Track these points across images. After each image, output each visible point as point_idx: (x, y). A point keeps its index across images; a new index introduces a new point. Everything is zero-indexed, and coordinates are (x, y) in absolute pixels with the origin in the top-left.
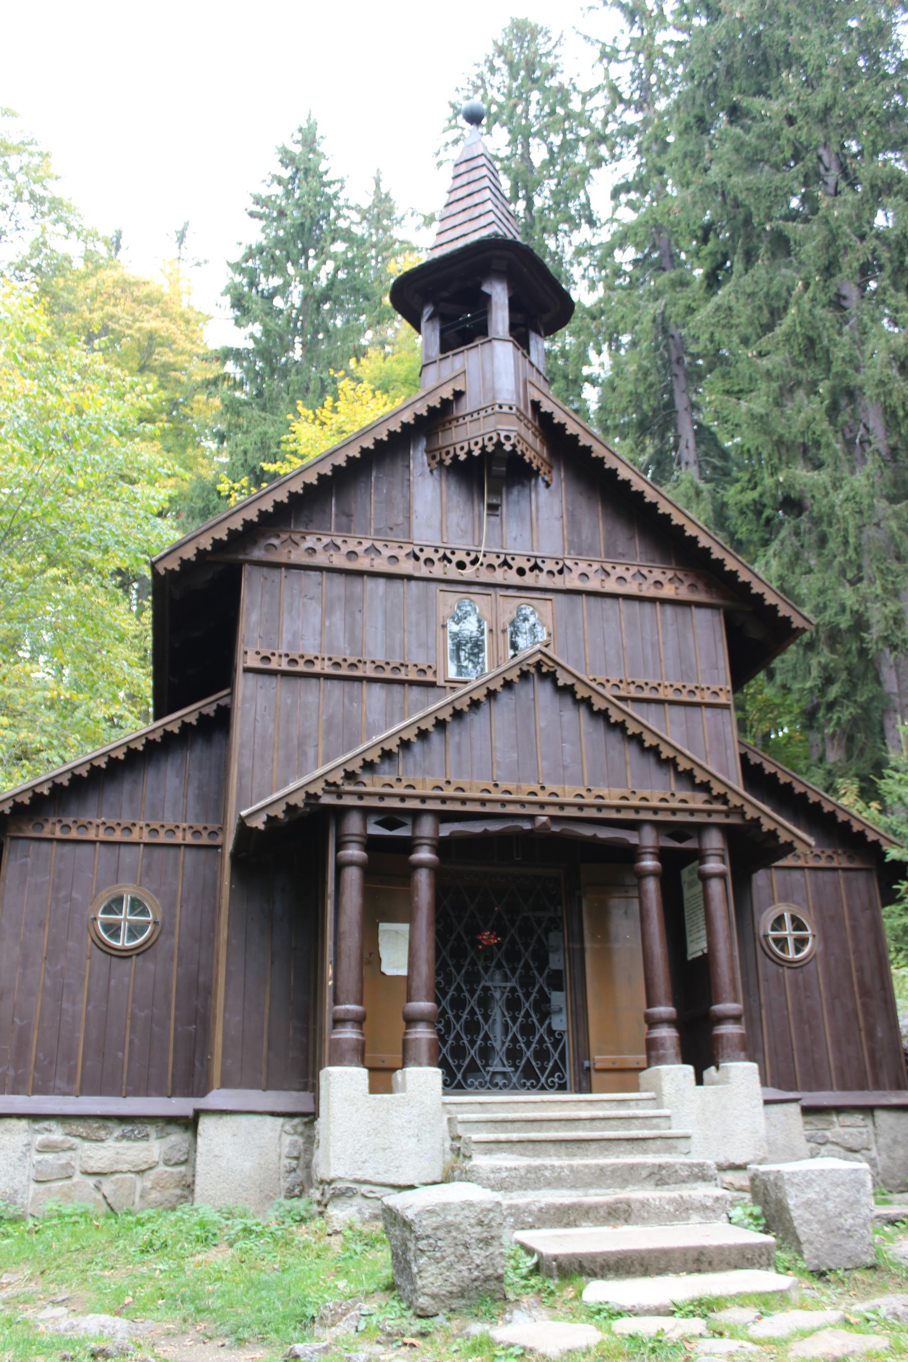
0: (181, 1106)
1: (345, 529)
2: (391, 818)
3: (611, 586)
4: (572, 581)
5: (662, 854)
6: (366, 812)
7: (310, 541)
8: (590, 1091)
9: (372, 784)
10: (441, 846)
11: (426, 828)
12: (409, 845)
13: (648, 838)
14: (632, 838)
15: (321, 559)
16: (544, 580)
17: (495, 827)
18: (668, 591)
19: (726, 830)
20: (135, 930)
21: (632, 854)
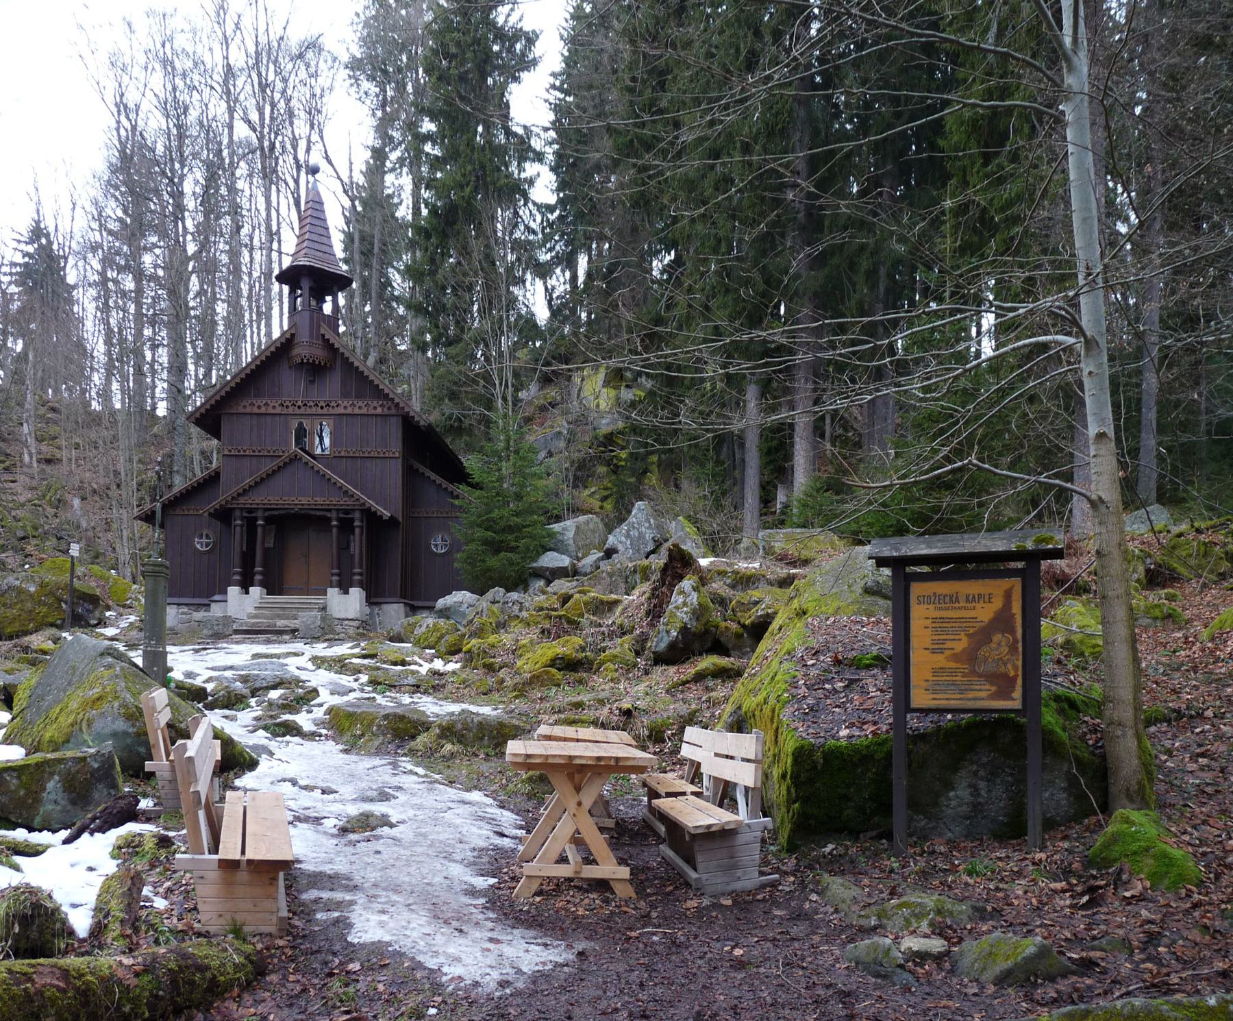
0: (206, 601)
1: (257, 396)
2: (250, 511)
3: (357, 411)
4: (341, 410)
5: (339, 519)
6: (242, 509)
7: (244, 403)
8: (281, 593)
9: (242, 500)
10: (266, 519)
11: (260, 514)
12: (330, 519)
13: (334, 515)
14: (329, 515)
15: (248, 410)
16: (332, 411)
17: (282, 512)
18: (379, 410)
19: (362, 511)
20: (207, 545)
21: (330, 519)
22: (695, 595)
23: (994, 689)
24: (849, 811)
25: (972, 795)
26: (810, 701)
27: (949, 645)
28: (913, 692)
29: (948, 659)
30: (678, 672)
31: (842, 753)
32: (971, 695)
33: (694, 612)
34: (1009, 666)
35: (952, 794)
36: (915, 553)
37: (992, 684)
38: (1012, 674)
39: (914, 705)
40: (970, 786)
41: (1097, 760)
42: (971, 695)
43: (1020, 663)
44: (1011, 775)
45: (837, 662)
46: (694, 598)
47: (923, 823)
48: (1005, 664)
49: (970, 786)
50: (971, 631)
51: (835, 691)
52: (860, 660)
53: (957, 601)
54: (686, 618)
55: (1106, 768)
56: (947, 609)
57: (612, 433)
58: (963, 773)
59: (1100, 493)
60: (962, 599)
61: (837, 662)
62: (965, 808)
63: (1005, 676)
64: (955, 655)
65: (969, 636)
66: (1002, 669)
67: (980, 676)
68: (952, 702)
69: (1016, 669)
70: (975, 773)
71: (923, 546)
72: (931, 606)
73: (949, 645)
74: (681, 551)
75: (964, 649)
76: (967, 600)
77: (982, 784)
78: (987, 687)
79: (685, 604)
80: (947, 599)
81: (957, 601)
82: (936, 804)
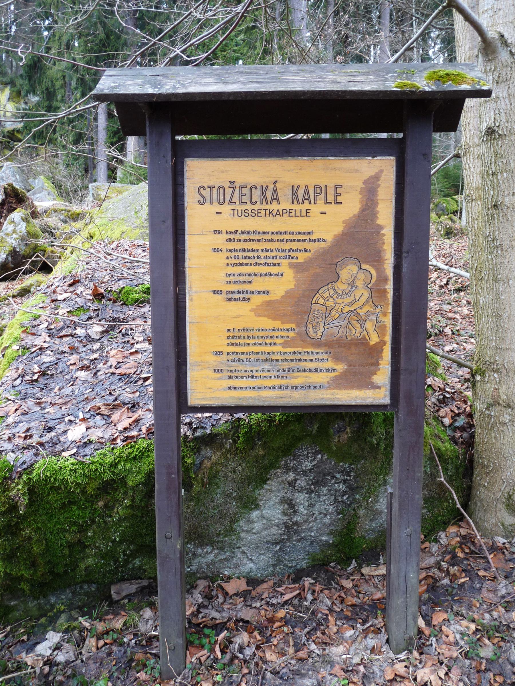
22: (24, 225)
23: (341, 367)
24: (91, 561)
25: (284, 514)
26: (48, 358)
27: (259, 284)
28: (192, 375)
29: (258, 312)
30: (7, 287)
31: (64, 482)
32: (300, 379)
33: (22, 239)
34: (369, 326)
35: (255, 514)
36: (191, 89)
37: (337, 359)
38: (374, 339)
39: (193, 400)
40: (283, 501)
41: (460, 450)
42: (300, 379)
43: (388, 320)
44: (345, 481)
45: (98, 296)
46: (23, 226)
47: (211, 557)
48: (362, 322)
49: (283, 501)
50: (302, 257)
51: (90, 339)
52: (128, 293)
53: (276, 198)
54: (15, 243)
55: (471, 461)
56: (257, 214)
57: (13, 131)
58: (273, 484)
59: (501, 29)
60: (285, 195)
61: (98, 296)
62: (274, 530)
63: (363, 342)
64: (268, 303)
65: (298, 268)
66: (357, 332)
67: (318, 344)
68: (265, 393)
69: (380, 329)
70: (292, 484)
71: (211, 80)
72: (226, 208)
73: (259, 284)
74: (14, 190)
75: (288, 294)
76: (295, 198)
77: (300, 498)
78: (329, 364)
79: (14, 232)
80: (257, 195)
81: (276, 198)
82: (230, 530)
